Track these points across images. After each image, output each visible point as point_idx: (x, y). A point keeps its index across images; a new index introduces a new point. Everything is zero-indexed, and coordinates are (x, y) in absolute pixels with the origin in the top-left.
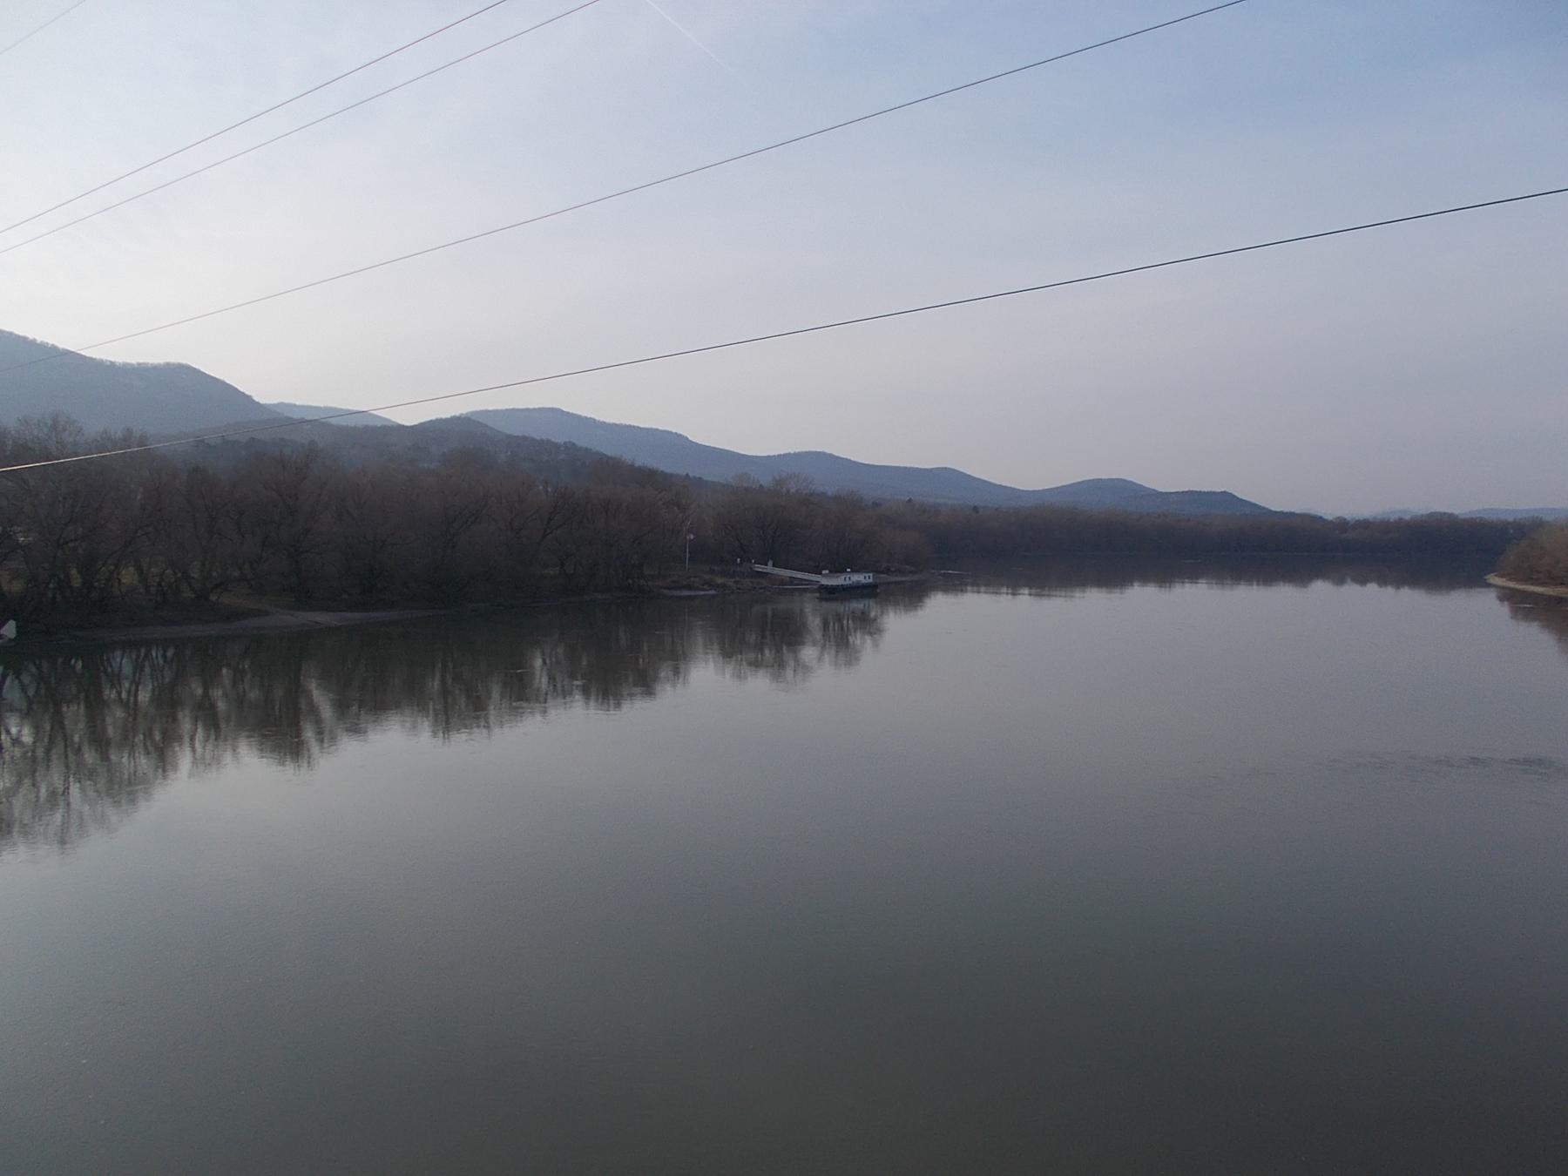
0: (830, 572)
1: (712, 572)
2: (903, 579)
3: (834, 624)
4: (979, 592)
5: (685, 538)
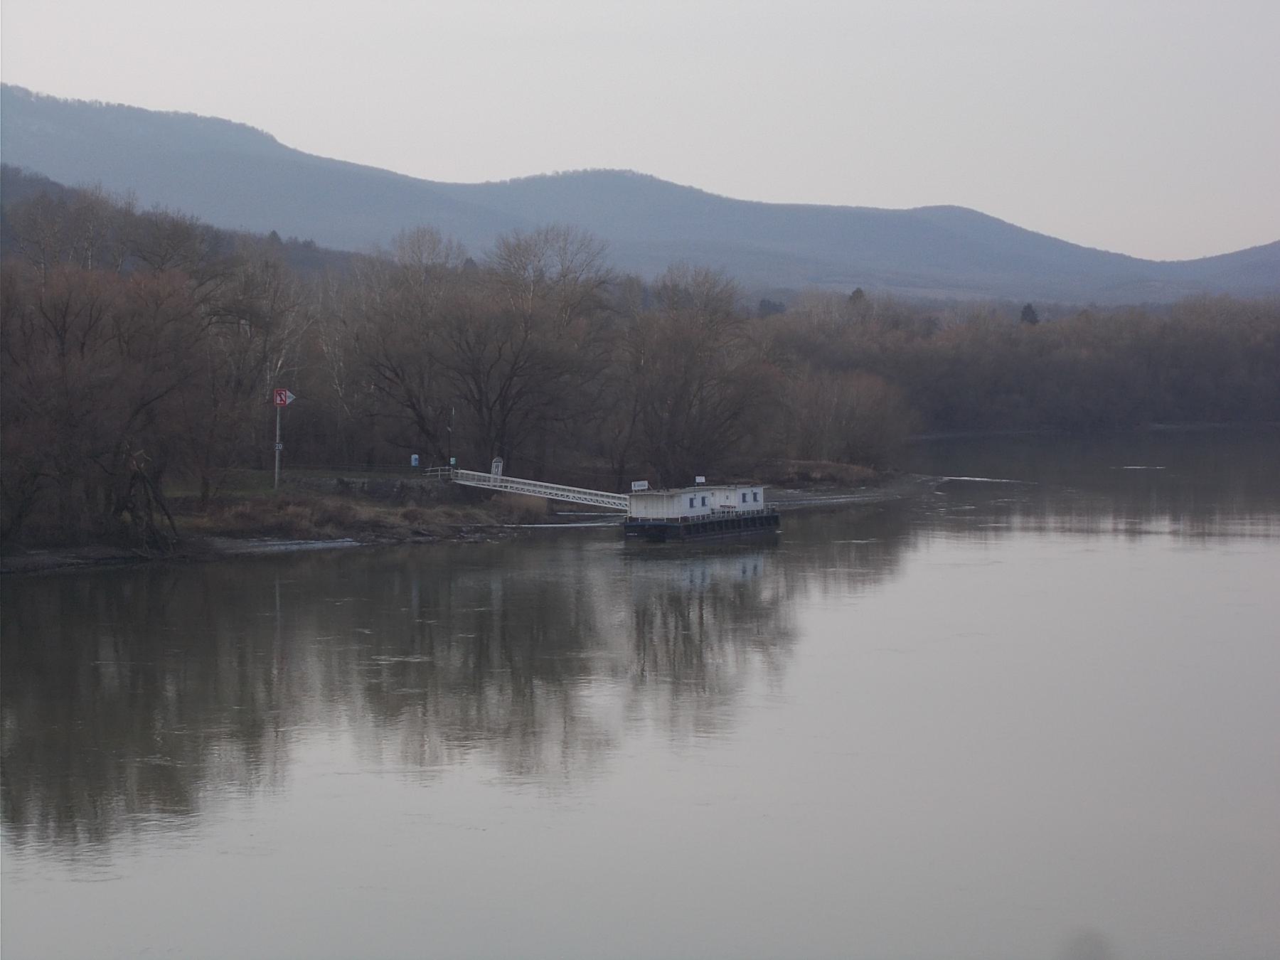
0: (653, 485)
1: (345, 489)
2: (842, 499)
3: (664, 615)
4: (1041, 529)
5: (272, 400)
